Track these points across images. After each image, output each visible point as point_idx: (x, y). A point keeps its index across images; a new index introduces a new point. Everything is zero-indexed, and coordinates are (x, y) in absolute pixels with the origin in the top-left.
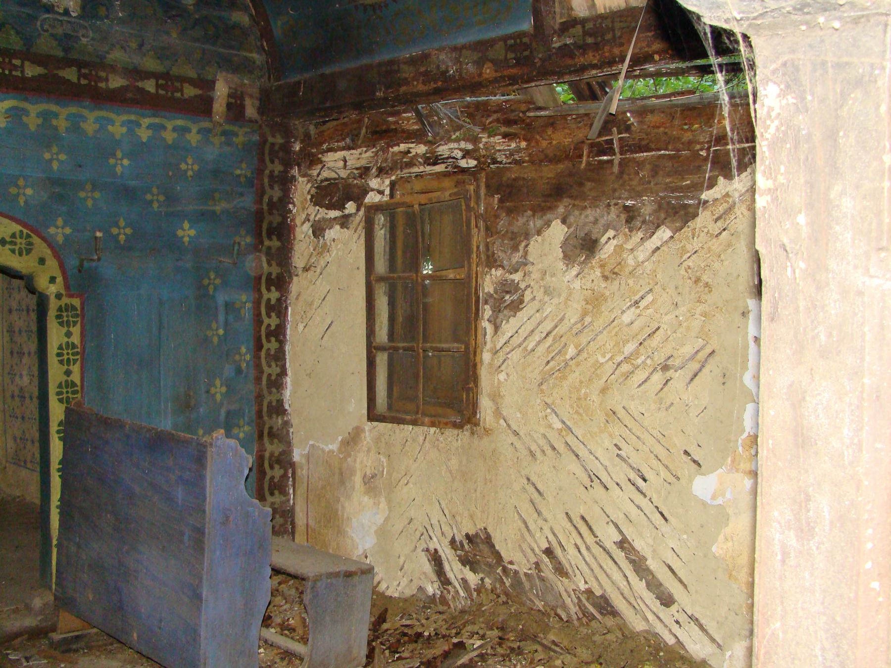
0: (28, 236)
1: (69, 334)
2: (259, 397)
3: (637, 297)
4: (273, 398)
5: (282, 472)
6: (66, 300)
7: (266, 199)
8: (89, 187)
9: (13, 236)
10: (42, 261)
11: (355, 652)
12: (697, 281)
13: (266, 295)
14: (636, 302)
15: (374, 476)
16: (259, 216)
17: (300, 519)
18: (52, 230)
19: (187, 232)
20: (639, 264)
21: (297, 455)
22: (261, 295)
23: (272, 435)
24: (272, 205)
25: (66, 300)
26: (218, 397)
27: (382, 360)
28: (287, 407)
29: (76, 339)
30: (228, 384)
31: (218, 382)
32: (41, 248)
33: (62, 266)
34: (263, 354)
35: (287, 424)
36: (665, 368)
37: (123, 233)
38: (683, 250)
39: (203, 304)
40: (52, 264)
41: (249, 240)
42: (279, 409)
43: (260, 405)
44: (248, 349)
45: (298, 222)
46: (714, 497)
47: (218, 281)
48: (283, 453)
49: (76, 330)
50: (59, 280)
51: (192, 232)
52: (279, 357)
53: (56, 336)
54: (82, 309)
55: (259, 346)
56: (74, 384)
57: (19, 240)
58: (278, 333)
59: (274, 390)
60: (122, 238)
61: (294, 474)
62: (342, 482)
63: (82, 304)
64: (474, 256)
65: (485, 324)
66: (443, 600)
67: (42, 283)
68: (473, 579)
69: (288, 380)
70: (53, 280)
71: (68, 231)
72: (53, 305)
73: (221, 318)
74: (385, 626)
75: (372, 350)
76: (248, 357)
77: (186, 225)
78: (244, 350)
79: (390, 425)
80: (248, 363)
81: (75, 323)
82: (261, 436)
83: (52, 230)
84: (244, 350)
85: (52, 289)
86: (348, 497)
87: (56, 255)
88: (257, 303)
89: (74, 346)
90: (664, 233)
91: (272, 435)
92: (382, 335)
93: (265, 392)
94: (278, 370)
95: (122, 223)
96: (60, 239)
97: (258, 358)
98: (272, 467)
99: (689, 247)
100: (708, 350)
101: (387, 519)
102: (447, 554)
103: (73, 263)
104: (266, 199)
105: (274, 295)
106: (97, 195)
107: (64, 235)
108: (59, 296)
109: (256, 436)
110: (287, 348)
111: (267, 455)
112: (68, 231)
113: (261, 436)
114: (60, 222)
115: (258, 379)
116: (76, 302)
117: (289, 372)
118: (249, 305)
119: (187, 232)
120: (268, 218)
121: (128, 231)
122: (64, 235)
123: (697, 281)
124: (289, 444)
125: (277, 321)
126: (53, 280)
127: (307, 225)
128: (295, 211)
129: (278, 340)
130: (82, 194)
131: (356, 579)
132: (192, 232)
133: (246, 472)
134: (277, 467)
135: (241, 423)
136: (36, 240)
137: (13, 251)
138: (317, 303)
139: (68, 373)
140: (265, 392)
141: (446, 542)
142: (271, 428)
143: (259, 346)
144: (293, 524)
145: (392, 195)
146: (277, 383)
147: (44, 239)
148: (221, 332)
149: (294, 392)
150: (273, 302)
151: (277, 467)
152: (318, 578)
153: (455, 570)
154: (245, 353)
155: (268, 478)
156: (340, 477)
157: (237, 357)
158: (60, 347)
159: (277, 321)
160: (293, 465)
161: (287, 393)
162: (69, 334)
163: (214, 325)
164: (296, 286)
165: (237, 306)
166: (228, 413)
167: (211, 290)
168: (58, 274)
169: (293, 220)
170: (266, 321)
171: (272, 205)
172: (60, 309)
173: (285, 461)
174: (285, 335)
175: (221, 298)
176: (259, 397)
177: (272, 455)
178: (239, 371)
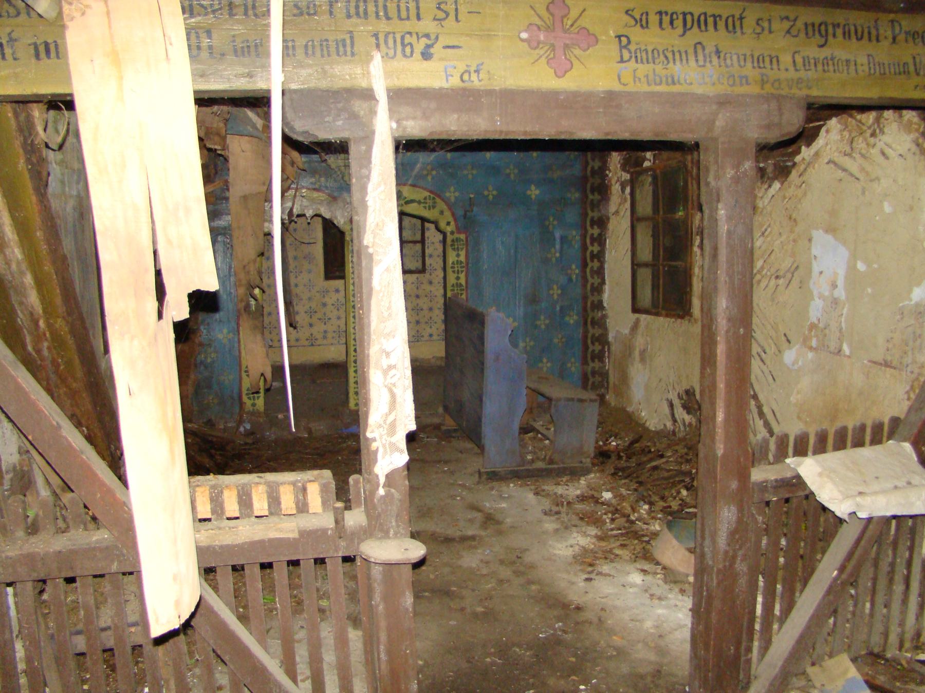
0: (434, 198)
1: (458, 255)
2: (585, 298)
3: (763, 230)
4: (596, 298)
5: (600, 347)
6: (456, 236)
7: (589, 169)
8: (469, 167)
9: (425, 198)
10: (442, 213)
11: (585, 449)
12: (790, 218)
13: (590, 231)
14: (763, 234)
15: (644, 350)
16: (585, 179)
17: (612, 379)
18: (448, 194)
19: (534, 192)
20: (764, 208)
21: (611, 338)
22: (586, 231)
23: (594, 323)
24: (593, 172)
25: (456, 236)
26: (555, 297)
27: (645, 275)
28: (605, 305)
29: (462, 258)
30: (562, 288)
31: (555, 287)
32: (441, 205)
33: (453, 215)
34: (588, 270)
35: (604, 317)
36: (777, 277)
37: (491, 193)
38: (784, 197)
39: (546, 238)
40: (447, 213)
41: (577, 195)
42: (599, 306)
43: (586, 303)
44: (577, 267)
45: (613, 182)
46: (793, 365)
47: (555, 223)
48: (601, 335)
49: (463, 253)
50: (452, 223)
51: (537, 192)
52: (600, 272)
53: (452, 257)
54: (467, 241)
55: (585, 265)
56: (461, 285)
57: (428, 201)
58: (600, 256)
59: (596, 294)
60: (491, 197)
61: (609, 349)
62: (630, 355)
63: (467, 238)
64: (690, 203)
65: (696, 249)
66: (674, 433)
67: (442, 225)
68: (687, 418)
69: (607, 288)
70: (448, 224)
71: (457, 194)
72: (449, 238)
73: (558, 246)
74: (637, 445)
75: (636, 265)
76: (577, 271)
77: (533, 187)
78: (574, 267)
79: (653, 317)
80: (577, 275)
81: (462, 249)
82: (585, 324)
83: (448, 194)
84: (574, 267)
85: (449, 229)
86: (632, 364)
87: (450, 209)
88: (584, 237)
89: (461, 262)
90: (777, 185)
91: (594, 323)
92: (646, 254)
93: (589, 294)
94: (600, 280)
95: (490, 188)
96: (453, 199)
97: (585, 272)
98: (593, 343)
99: (787, 195)
100: (795, 265)
101: (649, 378)
102: (677, 402)
103: (460, 212)
104: (589, 169)
105: (596, 231)
106: (475, 172)
107: (456, 197)
108: (452, 233)
109: (582, 322)
110: (606, 266)
111: (590, 335)
112: (457, 194)
113: (585, 324)
114: (452, 189)
115: (584, 286)
116: (463, 236)
117: (607, 282)
118: (578, 238)
119: (534, 192)
120: (591, 180)
121: (495, 193)
122: (456, 197)
123: (790, 218)
124: (606, 329)
125: (599, 248)
126: (448, 224)
127: (618, 184)
128: (610, 175)
129: (599, 261)
130: (465, 172)
131: (586, 404)
132: (537, 192)
133: (510, 332)
134: (597, 344)
135: (572, 313)
136: (438, 200)
137: (425, 207)
138: (621, 235)
139: (458, 278)
140: (589, 294)
141: (676, 394)
142: (593, 318)
143: (585, 265)
144: (608, 382)
145: (654, 163)
146: (598, 289)
147: (443, 200)
148: (558, 255)
149: (610, 295)
150: (595, 236)
151: (597, 344)
152: (558, 400)
153: (681, 414)
154: (575, 270)
155: (590, 350)
156: (628, 349)
157: (569, 271)
158: (453, 263)
159: (599, 248)
160: (608, 343)
161: (606, 296)
162: (458, 255)
163: (553, 250)
164: (611, 226)
165: (570, 237)
166: (562, 308)
167: (551, 227)
168: (451, 219)
169: (610, 181)
170: (590, 248)
171: (593, 172)
172: (453, 241)
173: (602, 340)
174: (604, 258)
175: (557, 234)
176: (585, 298)
177: (593, 335)
178: (570, 280)
